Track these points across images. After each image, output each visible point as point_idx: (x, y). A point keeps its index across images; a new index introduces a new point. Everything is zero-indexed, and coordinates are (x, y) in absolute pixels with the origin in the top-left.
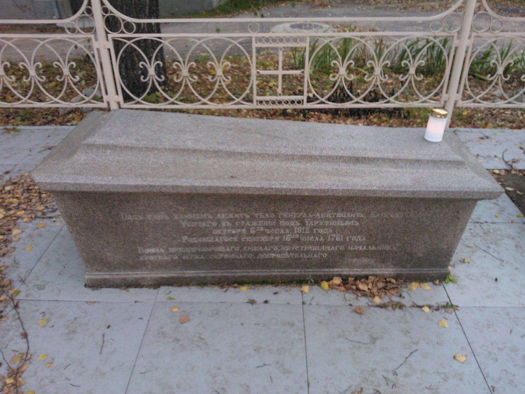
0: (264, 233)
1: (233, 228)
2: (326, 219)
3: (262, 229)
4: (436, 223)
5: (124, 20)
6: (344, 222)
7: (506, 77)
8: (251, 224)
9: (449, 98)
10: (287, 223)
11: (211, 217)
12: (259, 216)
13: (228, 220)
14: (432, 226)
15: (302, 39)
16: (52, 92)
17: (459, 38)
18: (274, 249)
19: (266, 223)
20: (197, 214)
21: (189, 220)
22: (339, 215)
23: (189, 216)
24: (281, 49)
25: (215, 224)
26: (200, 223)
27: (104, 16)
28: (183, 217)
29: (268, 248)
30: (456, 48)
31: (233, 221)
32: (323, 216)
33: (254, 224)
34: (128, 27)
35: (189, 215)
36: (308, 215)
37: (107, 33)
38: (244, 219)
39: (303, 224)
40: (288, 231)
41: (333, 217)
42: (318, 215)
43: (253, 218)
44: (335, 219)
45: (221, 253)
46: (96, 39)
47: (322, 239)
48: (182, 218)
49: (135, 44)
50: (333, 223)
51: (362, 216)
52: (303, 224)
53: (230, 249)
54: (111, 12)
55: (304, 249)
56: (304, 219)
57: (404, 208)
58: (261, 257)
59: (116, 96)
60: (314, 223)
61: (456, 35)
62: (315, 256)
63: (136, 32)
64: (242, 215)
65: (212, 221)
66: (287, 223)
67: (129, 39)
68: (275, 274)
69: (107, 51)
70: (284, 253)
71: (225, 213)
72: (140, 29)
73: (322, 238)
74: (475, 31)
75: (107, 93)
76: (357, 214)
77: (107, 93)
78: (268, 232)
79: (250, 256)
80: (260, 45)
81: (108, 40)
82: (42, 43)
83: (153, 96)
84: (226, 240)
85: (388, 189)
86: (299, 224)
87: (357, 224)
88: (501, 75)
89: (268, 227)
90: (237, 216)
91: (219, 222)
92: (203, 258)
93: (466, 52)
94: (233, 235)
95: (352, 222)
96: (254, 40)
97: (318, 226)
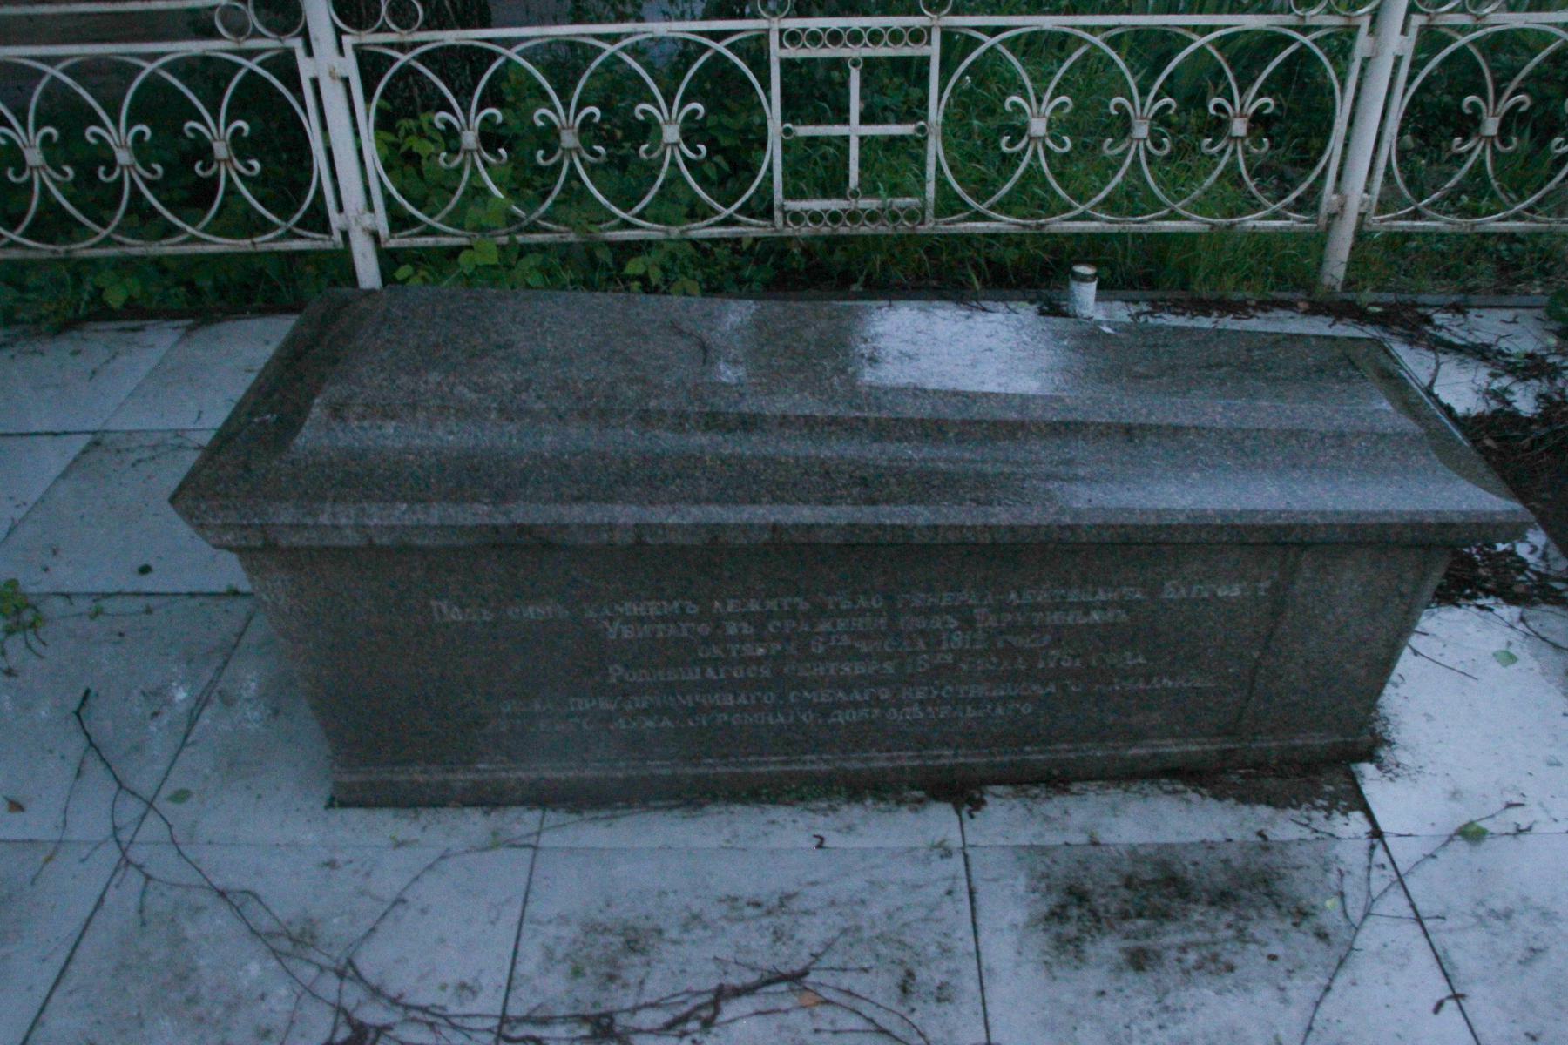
0: (851, 654)
1: (760, 639)
2: (1036, 607)
3: (846, 641)
6: (1087, 614)
8: (812, 626)
11: (692, 609)
12: (837, 605)
13: (744, 616)
14: (1330, 617)
15: (918, 36)
16: (692, 48)
18: (882, 697)
19: (859, 624)
20: (652, 603)
21: (627, 620)
22: (1074, 596)
23: (630, 608)
24: (855, 64)
26: (661, 626)
28: (612, 610)
29: (862, 693)
31: (760, 621)
32: (1027, 597)
33: (824, 626)
35: (627, 605)
36: (982, 598)
37: (339, 33)
38: (793, 613)
39: (968, 623)
40: (921, 645)
41: (1058, 600)
42: (1013, 596)
43: (820, 611)
44: (1062, 606)
45: (723, 709)
47: (1021, 665)
48: (607, 612)
49: (423, 63)
50: (1056, 618)
51: (1138, 595)
52: (968, 623)
53: (748, 698)
55: (967, 693)
56: (971, 608)
58: (841, 719)
60: (999, 621)
61: (1365, 23)
62: (1000, 711)
65: (698, 621)
66: (921, 623)
70: (910, 705)
71: (734, 597)
73: (1020, 660)
74: (1421, 12)
75: (340, 209)
76: (1125, 589)
77: (340, 209)
78: (864, 649)
86: (956, 624)
88: (677, 144)
89: (865, 636)
90: (772, 604)
91: (718, 622)
94: (758, 661)
96: (774, 39)
97: (1013, 628)
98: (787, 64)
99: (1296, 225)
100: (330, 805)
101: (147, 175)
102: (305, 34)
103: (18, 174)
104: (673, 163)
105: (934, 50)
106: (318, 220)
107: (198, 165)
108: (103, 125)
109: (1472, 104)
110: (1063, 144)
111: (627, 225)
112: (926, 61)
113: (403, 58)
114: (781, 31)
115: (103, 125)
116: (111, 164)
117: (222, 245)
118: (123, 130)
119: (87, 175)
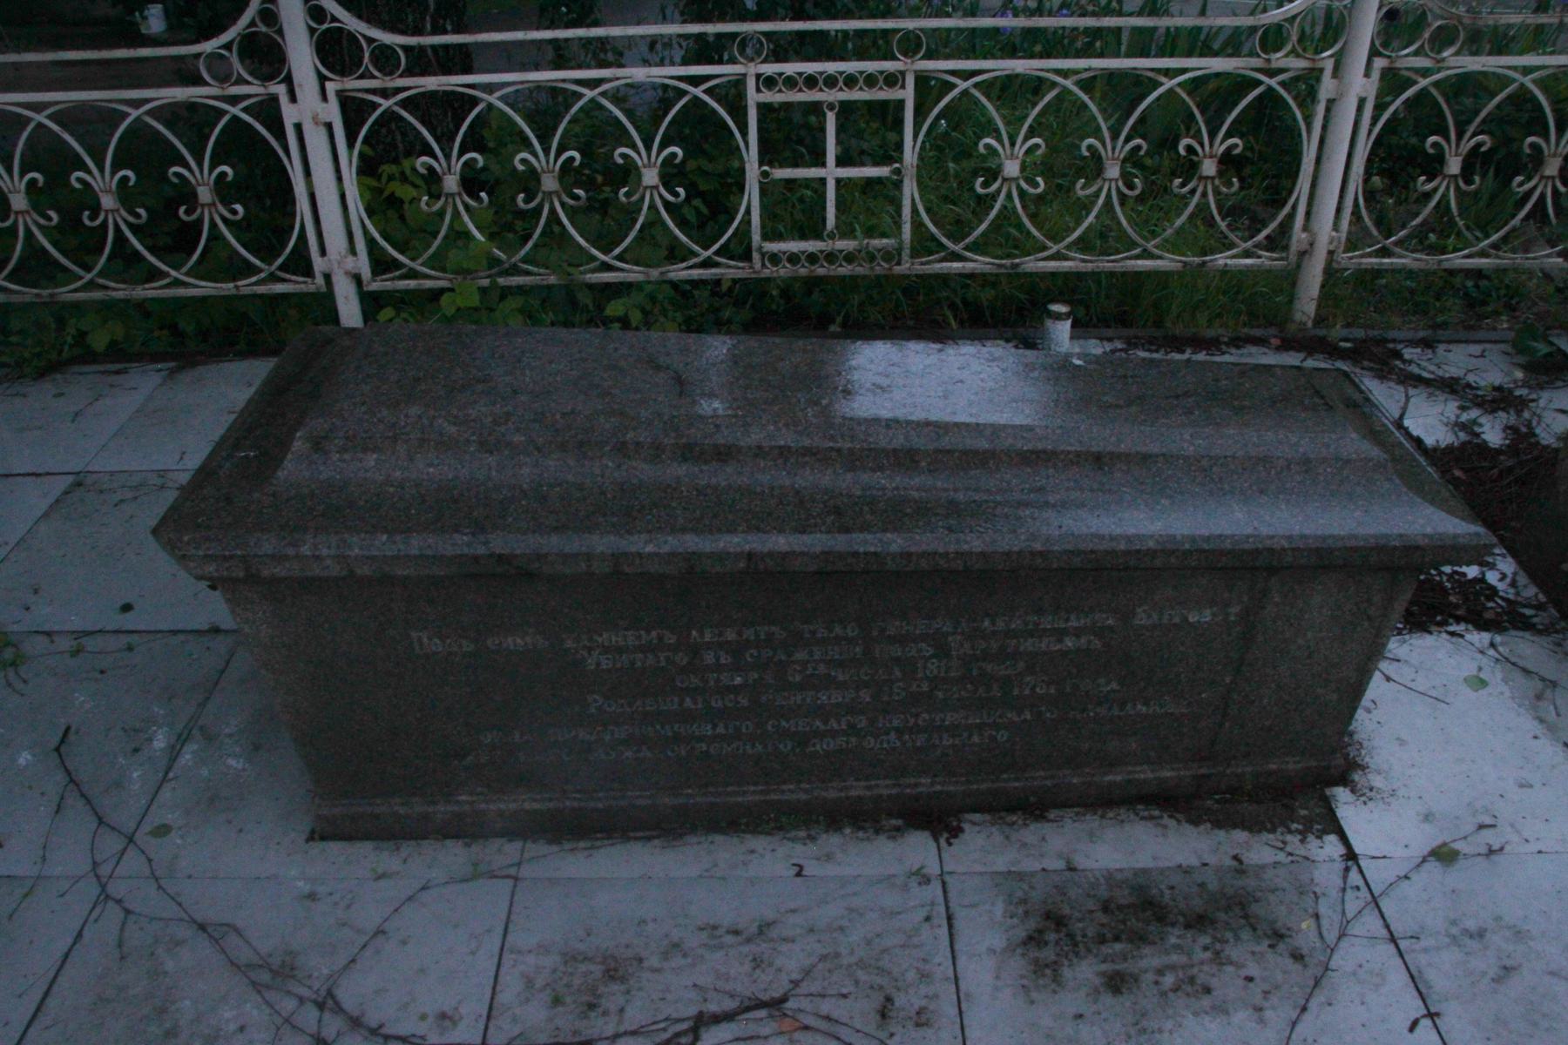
3: (822, 669)
4: (1309, 635)
5: (370, 40)
6: (1060, 641)
7: (1468, 182)
9: (1311, 245)
10: (897, 651)
11: (671, 639)
15: (892, 80)
17: (1337, 72)
21: (606, 650)
22: (1047, 622)
25: (682, 659)
27: (312, 31)
29: (839, 723)
30: (1331, 103)
32: (1000, 625)
33: (800, 655)
34: (385, 59)
37: (322, 79)
45: (701, 739)
46: (293, 98)
49: (405, 108)
50: (1029, 645)
52: (943, 651)
53: (726, 728)
54: (337, 20)
57: (1226, 595)
59: (350, 259)
61: (1329, 66)
62: (976, 739)
63: (409, 72)
64: (763, 631)
66: (897, 651)
67: (384, 93)
68: (853, 793)
69: (323, 132)
72: (420, 62)
73: (995, 687)
77: (323, 252)
79: (786, 747)
80: (769, 97)
81: (324, 98)
82: (134, 114)
83: (455, 257)
84: (717, 703)
85: (1187, 546)
87: (1097, 644)
89: (841, 664)
90: (749, 634)
92: (649, 754)
93: (1360, 109)
94: (735, 690)
95: (1083, 640)
96: (751, 83)
98: (764, 109)
99: (1267, 263)
100: (311, 838)
101: (131, 219)
102: (289, 80)
103: (93, 218)
104: (652, 207)
105: (908, 94)
106: (300, 264)
107: (182, 209)
108: (89, 172)
109: (1435, 145)
110: (1036, 185)
111: (607, 267)
112: (901, 104)
113: (385, 104)
114: (758, 76)
115: (89, 172)
116: (96, 210)
117: (206, 288)
118: (16, 178)
119: (71, 222)
